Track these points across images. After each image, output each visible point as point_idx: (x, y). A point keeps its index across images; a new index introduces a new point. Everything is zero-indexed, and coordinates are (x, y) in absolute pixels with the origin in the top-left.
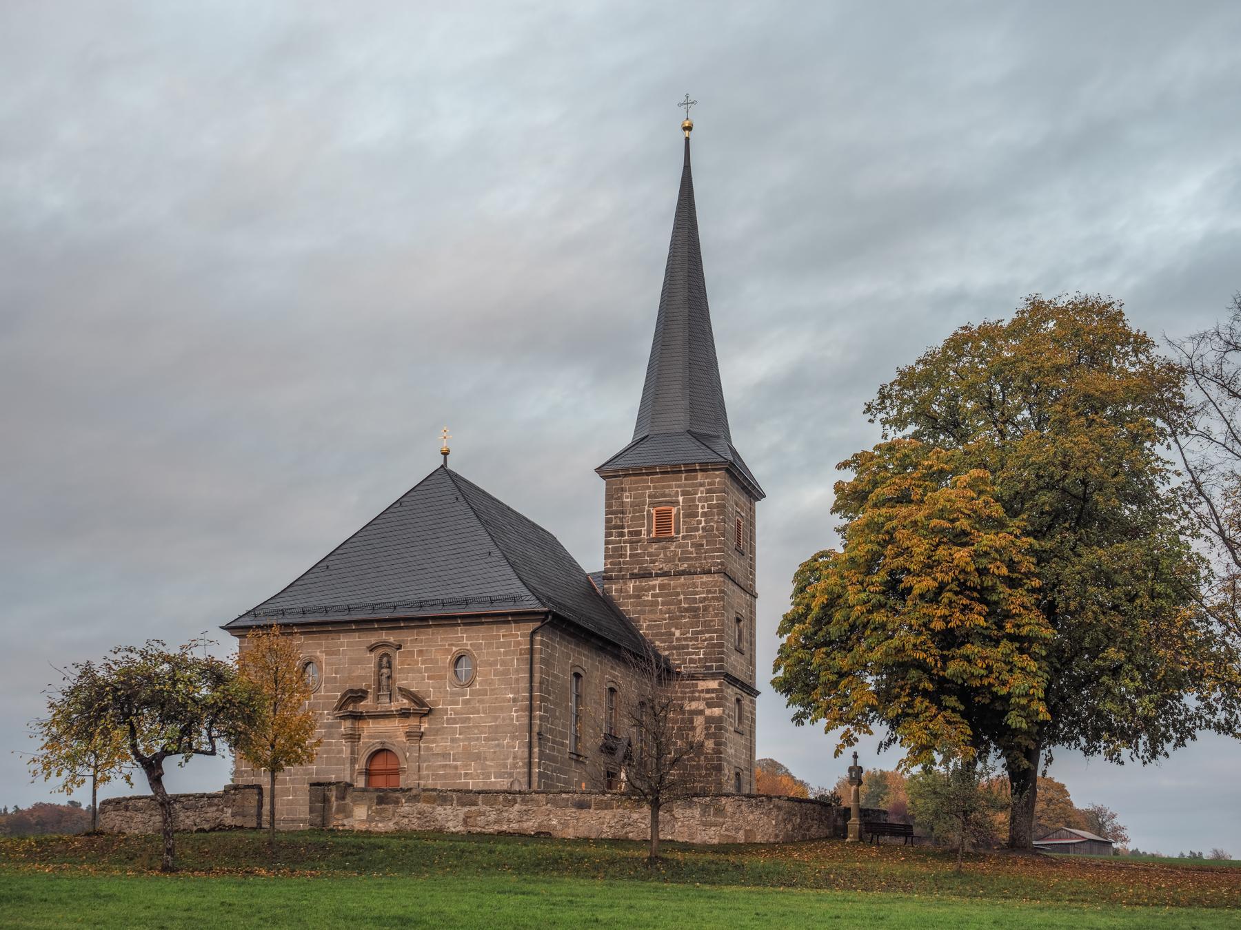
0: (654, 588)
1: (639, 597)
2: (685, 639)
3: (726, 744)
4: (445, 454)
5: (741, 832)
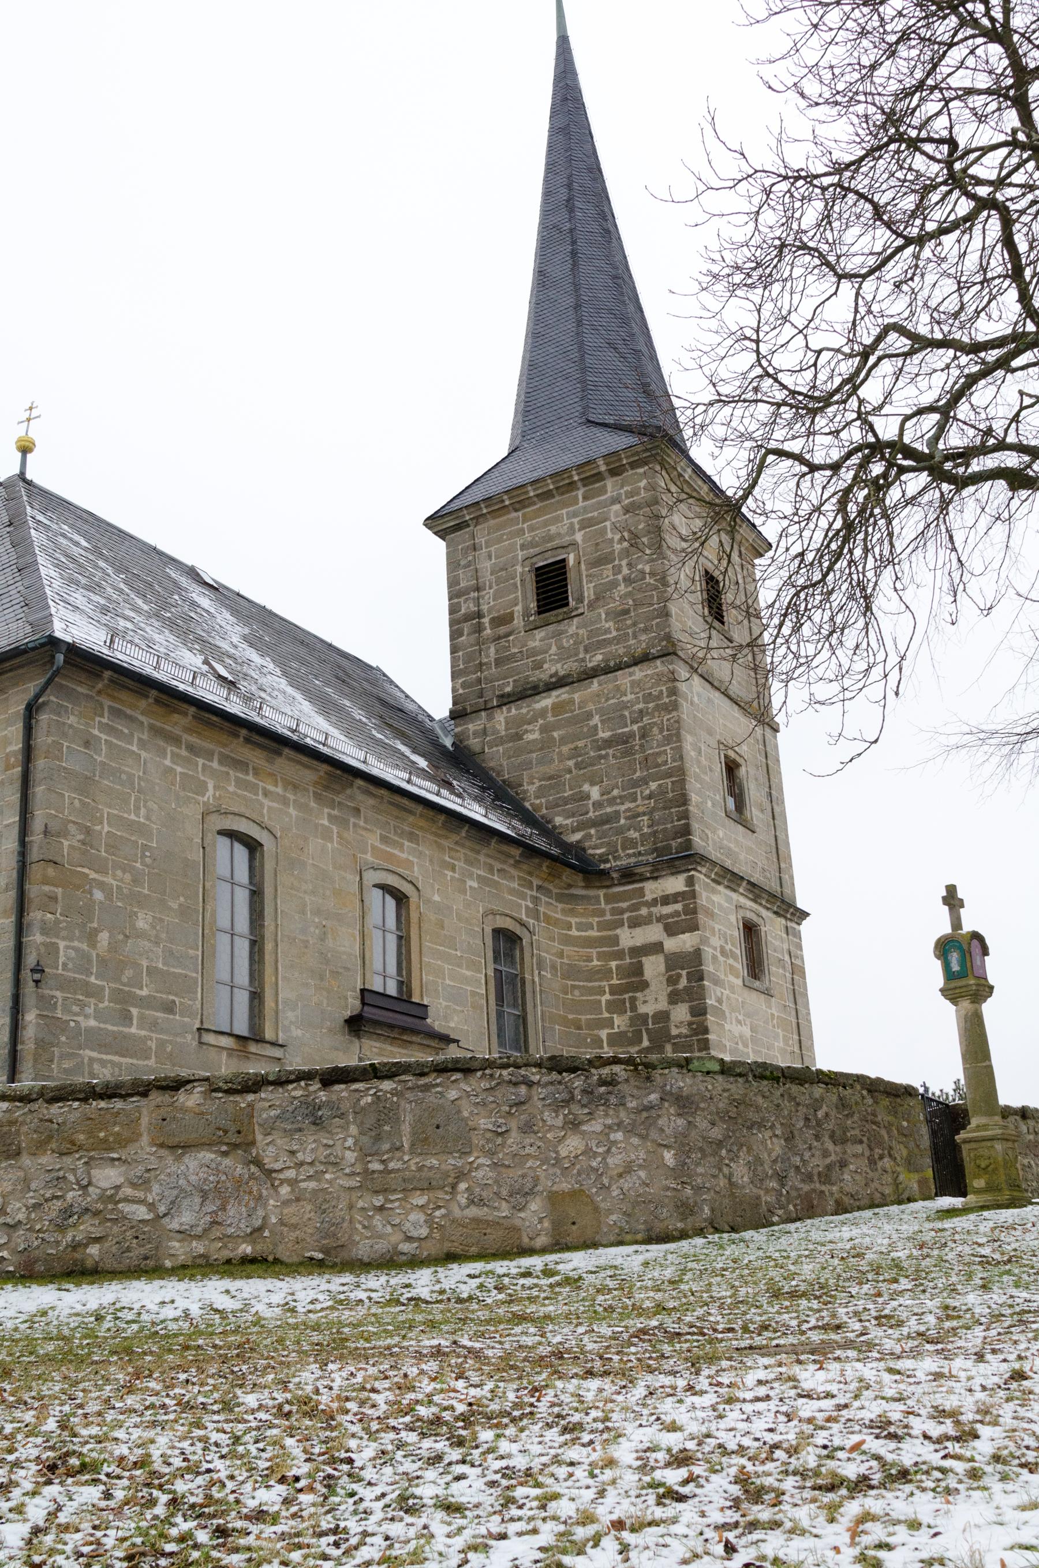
0: (543, 713)
1: (518, 737)
2: (612, 801)
4: (25, 450)
5: (535, 1205)
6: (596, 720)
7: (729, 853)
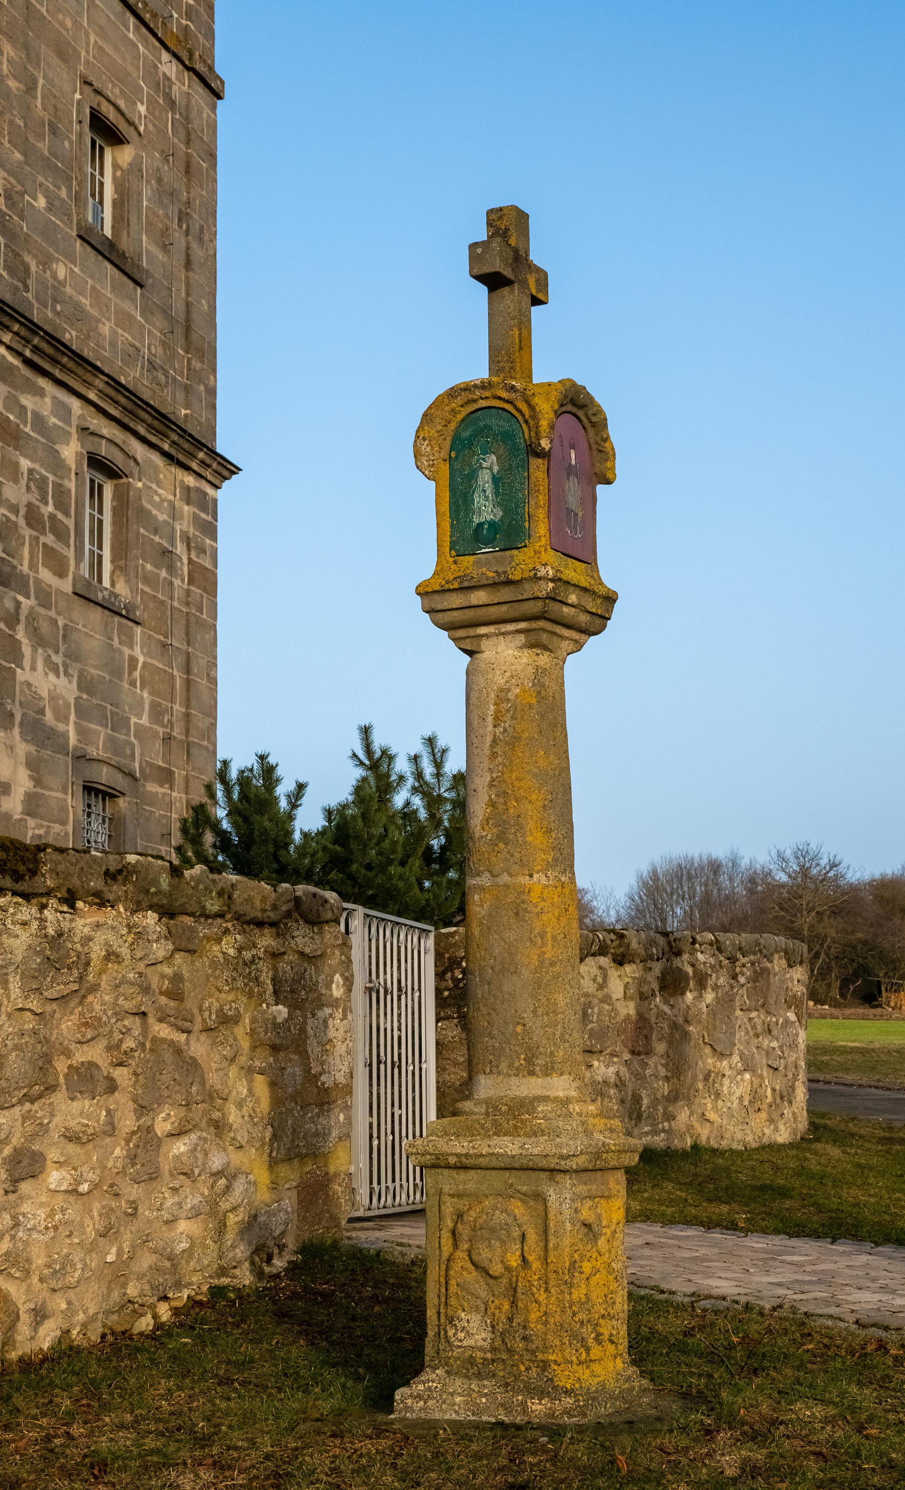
7: (78, 315)
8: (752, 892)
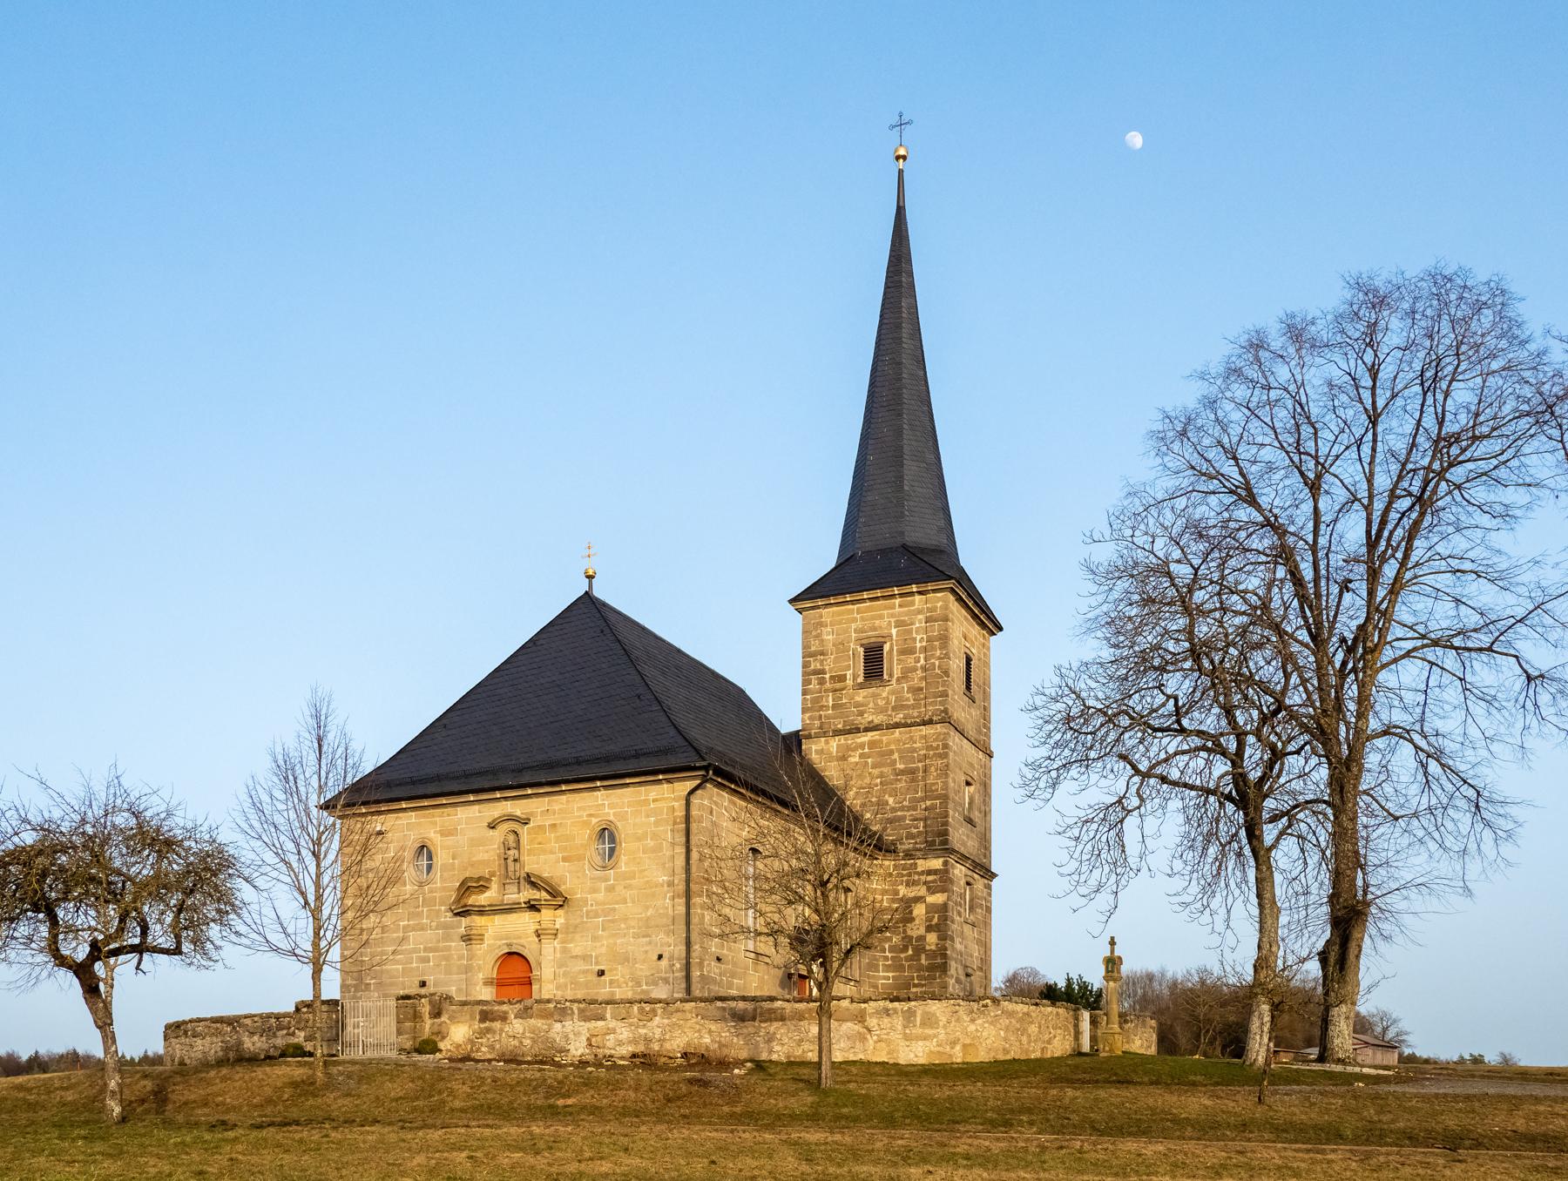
0: (862, 746)
2: (902, 809)
3: (952, 940)
5: (958, 1047)
6: (896, 756)
8: (1172, 994)
